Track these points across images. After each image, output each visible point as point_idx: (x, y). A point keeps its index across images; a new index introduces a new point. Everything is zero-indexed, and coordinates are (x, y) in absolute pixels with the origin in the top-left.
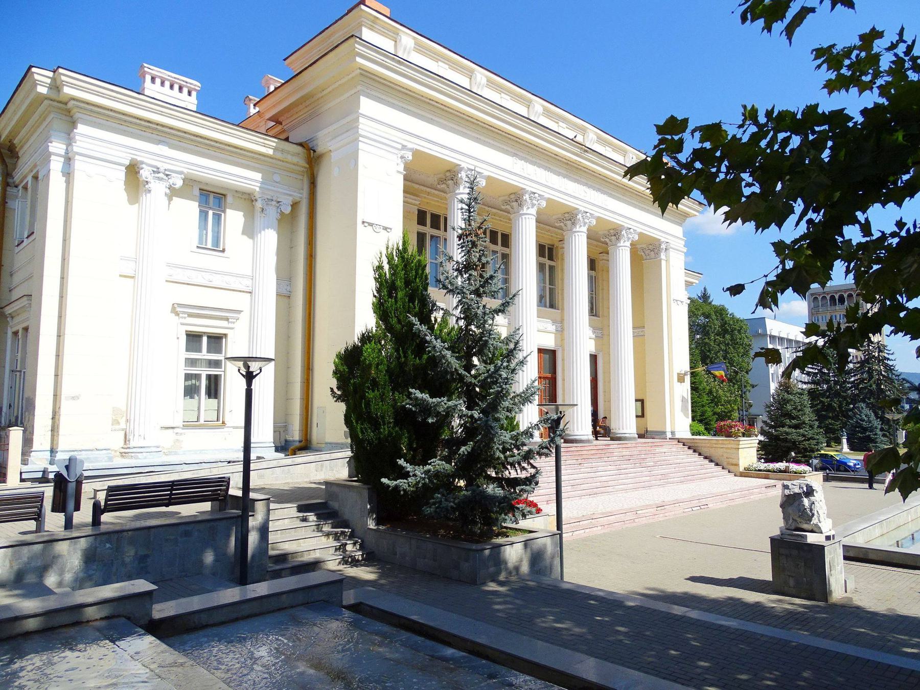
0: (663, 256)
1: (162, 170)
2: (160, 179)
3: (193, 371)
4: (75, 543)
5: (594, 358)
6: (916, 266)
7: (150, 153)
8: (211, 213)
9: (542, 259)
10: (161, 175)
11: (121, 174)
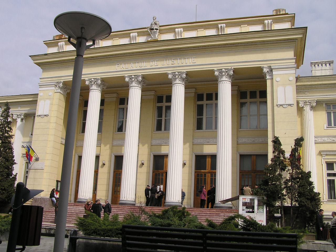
10: (19, 116)
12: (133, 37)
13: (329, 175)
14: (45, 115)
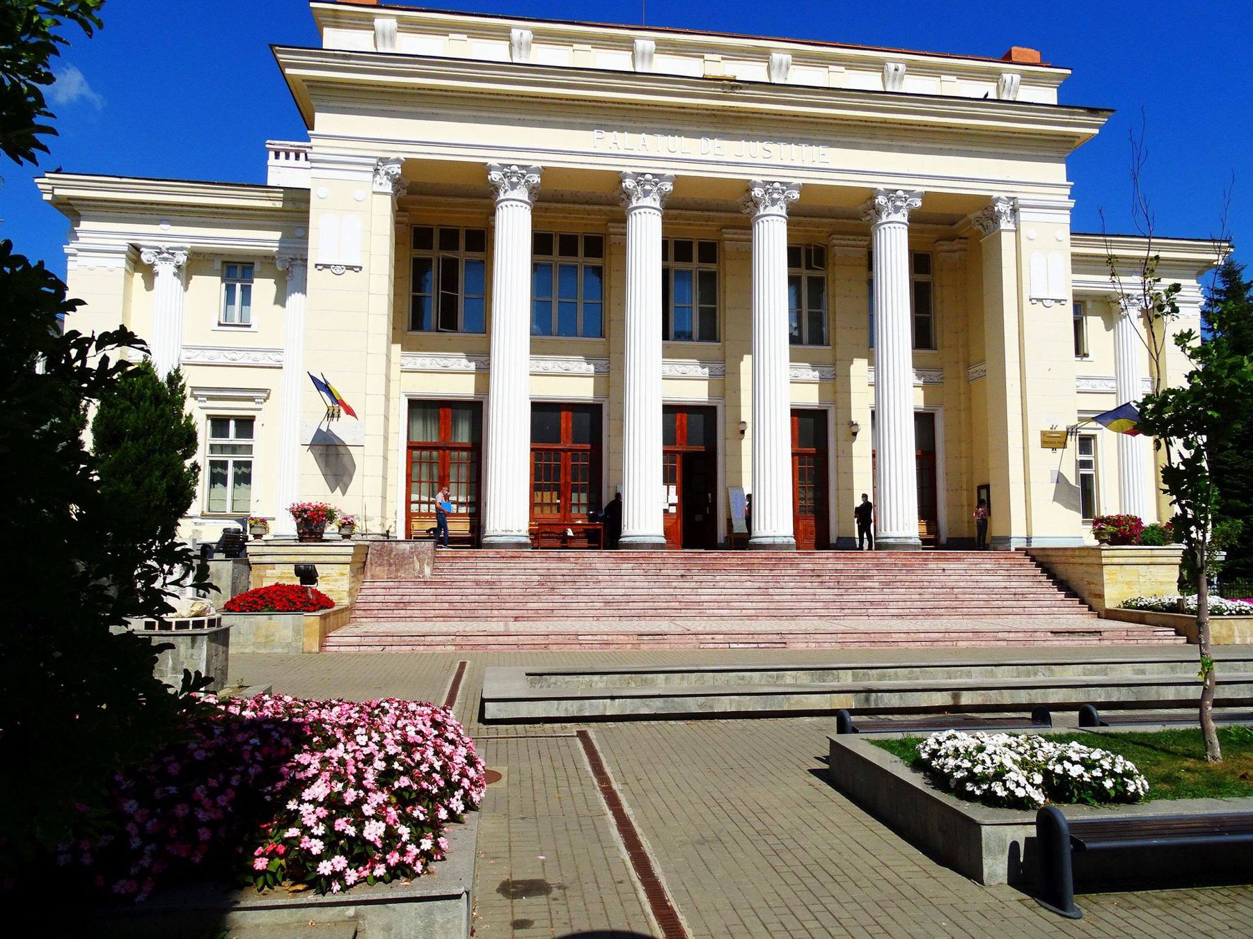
0: (1005, 224)
1: (164, 249)
2: (165, 259)
3: (219, 457)
4: (683, 679)
5: (924, 421)
6: (1096, 131)
7: (149, 234)
8: (238, 286)
9: (796, 270)
10: (165, 255)
11: (121, 262)
12: (781, 65)
13: (249, 449)
14: (350, 268)
